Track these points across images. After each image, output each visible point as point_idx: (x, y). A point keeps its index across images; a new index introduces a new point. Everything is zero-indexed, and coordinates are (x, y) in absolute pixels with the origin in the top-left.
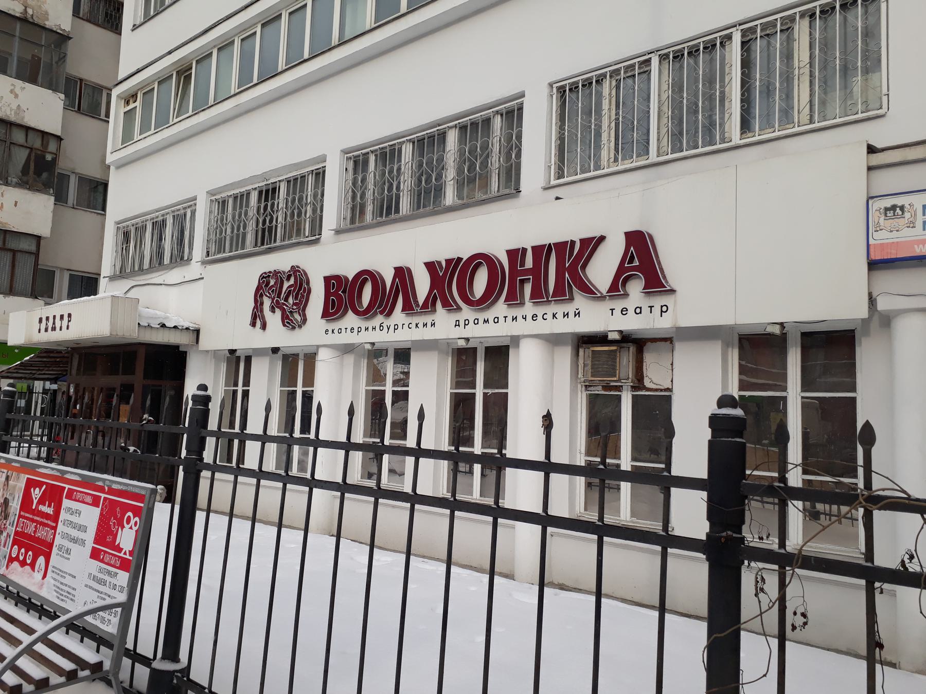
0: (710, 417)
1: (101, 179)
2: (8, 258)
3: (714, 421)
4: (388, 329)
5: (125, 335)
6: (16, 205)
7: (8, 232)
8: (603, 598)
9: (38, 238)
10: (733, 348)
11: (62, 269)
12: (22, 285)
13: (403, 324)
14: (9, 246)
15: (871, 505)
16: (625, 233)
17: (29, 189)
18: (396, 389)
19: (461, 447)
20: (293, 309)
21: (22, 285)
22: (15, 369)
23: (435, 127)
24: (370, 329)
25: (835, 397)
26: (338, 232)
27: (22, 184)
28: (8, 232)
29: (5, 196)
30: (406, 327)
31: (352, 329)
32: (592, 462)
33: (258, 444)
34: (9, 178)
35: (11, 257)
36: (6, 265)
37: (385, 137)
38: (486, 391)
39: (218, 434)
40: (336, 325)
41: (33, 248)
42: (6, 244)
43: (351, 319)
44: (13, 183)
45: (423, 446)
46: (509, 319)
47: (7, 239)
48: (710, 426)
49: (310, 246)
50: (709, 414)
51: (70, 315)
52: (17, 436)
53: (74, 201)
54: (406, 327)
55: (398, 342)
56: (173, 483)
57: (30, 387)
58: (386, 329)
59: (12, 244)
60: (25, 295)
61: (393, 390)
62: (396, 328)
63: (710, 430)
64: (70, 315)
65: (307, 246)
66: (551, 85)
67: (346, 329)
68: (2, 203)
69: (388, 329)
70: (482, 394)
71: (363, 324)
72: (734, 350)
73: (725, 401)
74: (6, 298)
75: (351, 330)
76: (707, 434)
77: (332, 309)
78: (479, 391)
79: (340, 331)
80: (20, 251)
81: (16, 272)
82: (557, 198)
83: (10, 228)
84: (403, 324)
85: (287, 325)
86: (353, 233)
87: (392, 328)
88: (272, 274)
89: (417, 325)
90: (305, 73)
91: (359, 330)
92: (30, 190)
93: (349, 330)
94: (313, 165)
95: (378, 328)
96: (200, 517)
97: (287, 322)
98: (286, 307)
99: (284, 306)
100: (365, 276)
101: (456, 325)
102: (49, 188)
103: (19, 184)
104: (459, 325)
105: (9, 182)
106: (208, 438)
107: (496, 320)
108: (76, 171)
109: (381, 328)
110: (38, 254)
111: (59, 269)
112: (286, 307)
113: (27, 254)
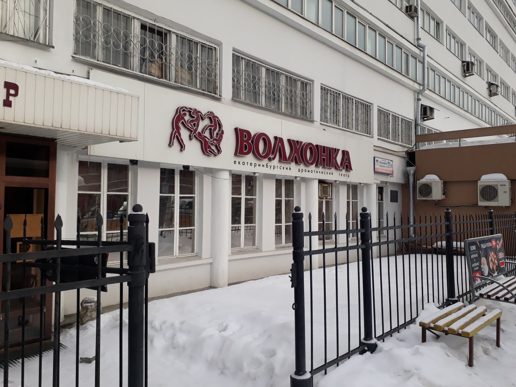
4: (271, 167)
10: (104, 169)
13: (277, 166)
18: (247, 197)
19: (81, 232)
20: (214, 142)
24: (261, 166)
25: (186, 197)
30: (279, 167)
31: (251, 164)
32: (183, 231)
33: (313, 230)
37: (265, 61)
38: (286, 199)
39: (186, 232)
40: (241, 160)
43: (250, 158)
46: (315, 172)
49: (213, 100)
54: (279, 167)
55: (121, 159)
58: (269, 167)
61: (78, 194)
62: (302, 171)
65: (210, 99)
66: (313, 81)
67: (247, 163)
69: (271, 167)
70: (284, 200)
71: (258, 163)
72: (105, 169)
75: (250, 164)
77: (245, 150)
78: (104, 193)
79: (305, 171)
82: (324, 130)
84: (277, 166)
85: (210, 153)
86: (303, 121)
87: (272, 167)
88: (192, 111)
89: (283, 168)
90: (274, 9)
91: (255, 165)
93: (249, 164)
94: (202, 39)
95: (265, 166)
96: (306, 275)
97: (209, 151)
98: (207, 140)
99: (206, 139)
100: (264, 137)
101: (299, 171)
104: (300, 171)
106: (62, 239)
107: (244, 163)
109: (267, 166)
112: (207, 140)
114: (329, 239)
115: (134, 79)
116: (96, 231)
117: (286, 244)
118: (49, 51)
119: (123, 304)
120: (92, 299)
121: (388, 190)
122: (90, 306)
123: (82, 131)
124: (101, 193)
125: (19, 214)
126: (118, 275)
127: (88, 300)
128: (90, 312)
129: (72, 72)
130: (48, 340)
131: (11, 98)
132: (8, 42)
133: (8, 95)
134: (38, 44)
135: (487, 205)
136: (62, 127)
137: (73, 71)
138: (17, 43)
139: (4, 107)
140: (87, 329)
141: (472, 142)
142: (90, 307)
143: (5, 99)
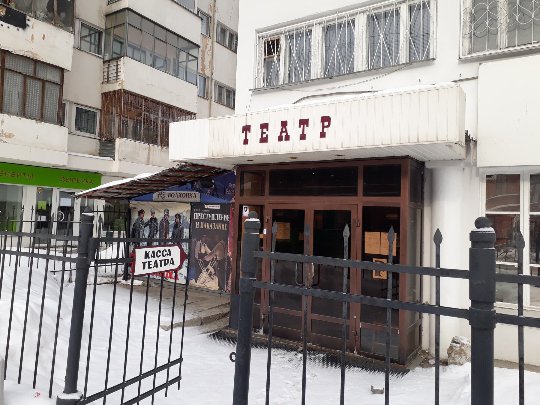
0: (470, 233)
1: (99, 27)
2: (38, 87)
3: (473, 236)
5: (229, 155)
6: (44, 38)
7: (38, 63)
8: (497, 367)
9: (62, 70)
11: (71, 103)
12: (50, 113)
14: (39, 76)
15: (74, 278)
16: (287, 121)
17: (54, 25)
21: (50, 113)
22: (128, 186)
23: (336, 13)
26: (256, 91)
27: (48, 20)
28: (38, 63)
29: (34, 29)
34: (38, 12)
35: (41, 87)
36: (37, 91)
41: (57, 80)
42: (37, 74)
44: (41, 17)
45: (39, 253)
47: (37, 68)
48: (471, 240)
50: (470, 232)
51: (326, 119)
52: (71, 252)
53: (78, 44)
56: (281, 293)
57: (48, 205)
59: (41, 74)
60: (53, 122)
63: (471, 242)
64: (326, 119)
68: (32, 34)
73: (479, 223)
74: (38, 123)
76: (469, 244)
80: (49, 82)
81: (45, 100)
83: (40, 59)
92: (55, 26)
102: (70, 26)
103: (46, 19)
105: (38, 16)
108: (81, 17)
110: (62, 86)
111: (68, 103)
113: (53, 85)
114: (502, 301)
115: (518, 57)
116: (515, 261)
117: (531, 306)
118: (434, 64)
119: (494, 361)
120: (459, 340)
121: (519, 182)
122: (455, 347)
123: (386, 145)
124: (521, 213)
125: (375, 232)
126: (96, 258)
127: (456, 340)
128: (454, 354)
129: (459, 76)
130: (402, 366)
131: (326, 130)
132: (395, 73)
133: (324, 127)
134: (418, 63)
135: (515, 214)
136: (419, 141)
137: (460, 74)
138: (402, 70)
139: (244, 145)
140: (446, 371)
141: (234, 43)
142: (454, 348)
143: (245, 139)
